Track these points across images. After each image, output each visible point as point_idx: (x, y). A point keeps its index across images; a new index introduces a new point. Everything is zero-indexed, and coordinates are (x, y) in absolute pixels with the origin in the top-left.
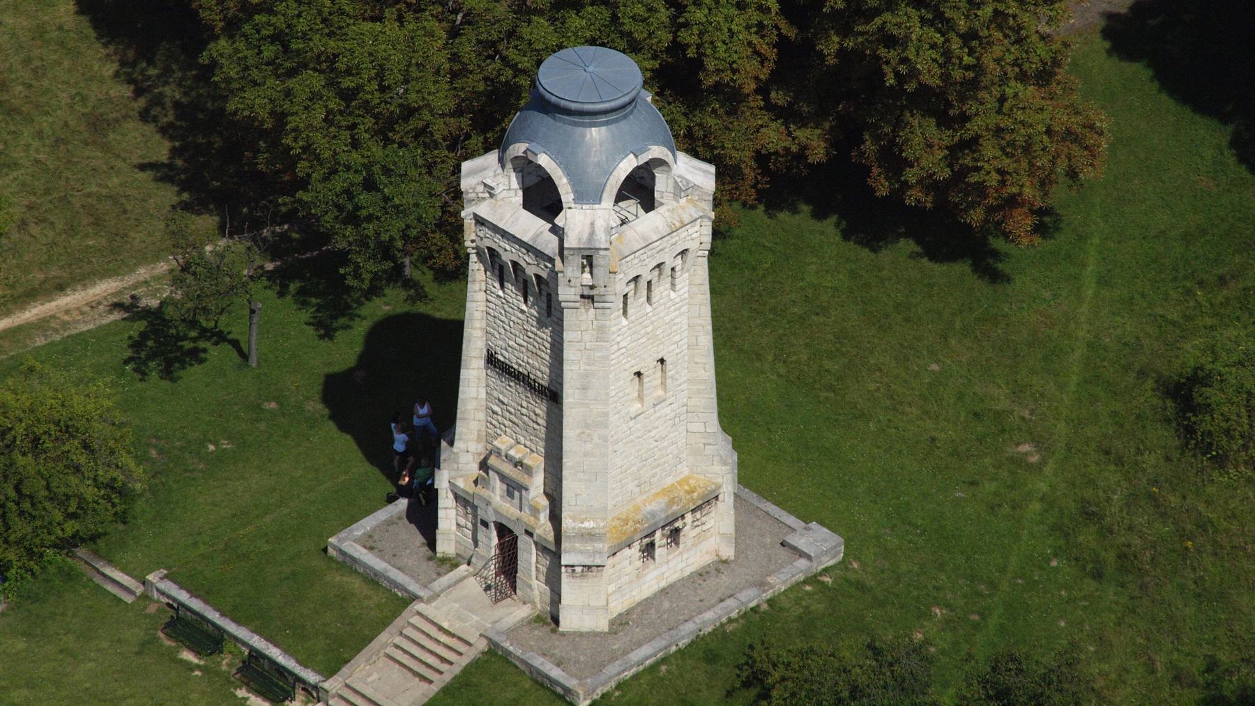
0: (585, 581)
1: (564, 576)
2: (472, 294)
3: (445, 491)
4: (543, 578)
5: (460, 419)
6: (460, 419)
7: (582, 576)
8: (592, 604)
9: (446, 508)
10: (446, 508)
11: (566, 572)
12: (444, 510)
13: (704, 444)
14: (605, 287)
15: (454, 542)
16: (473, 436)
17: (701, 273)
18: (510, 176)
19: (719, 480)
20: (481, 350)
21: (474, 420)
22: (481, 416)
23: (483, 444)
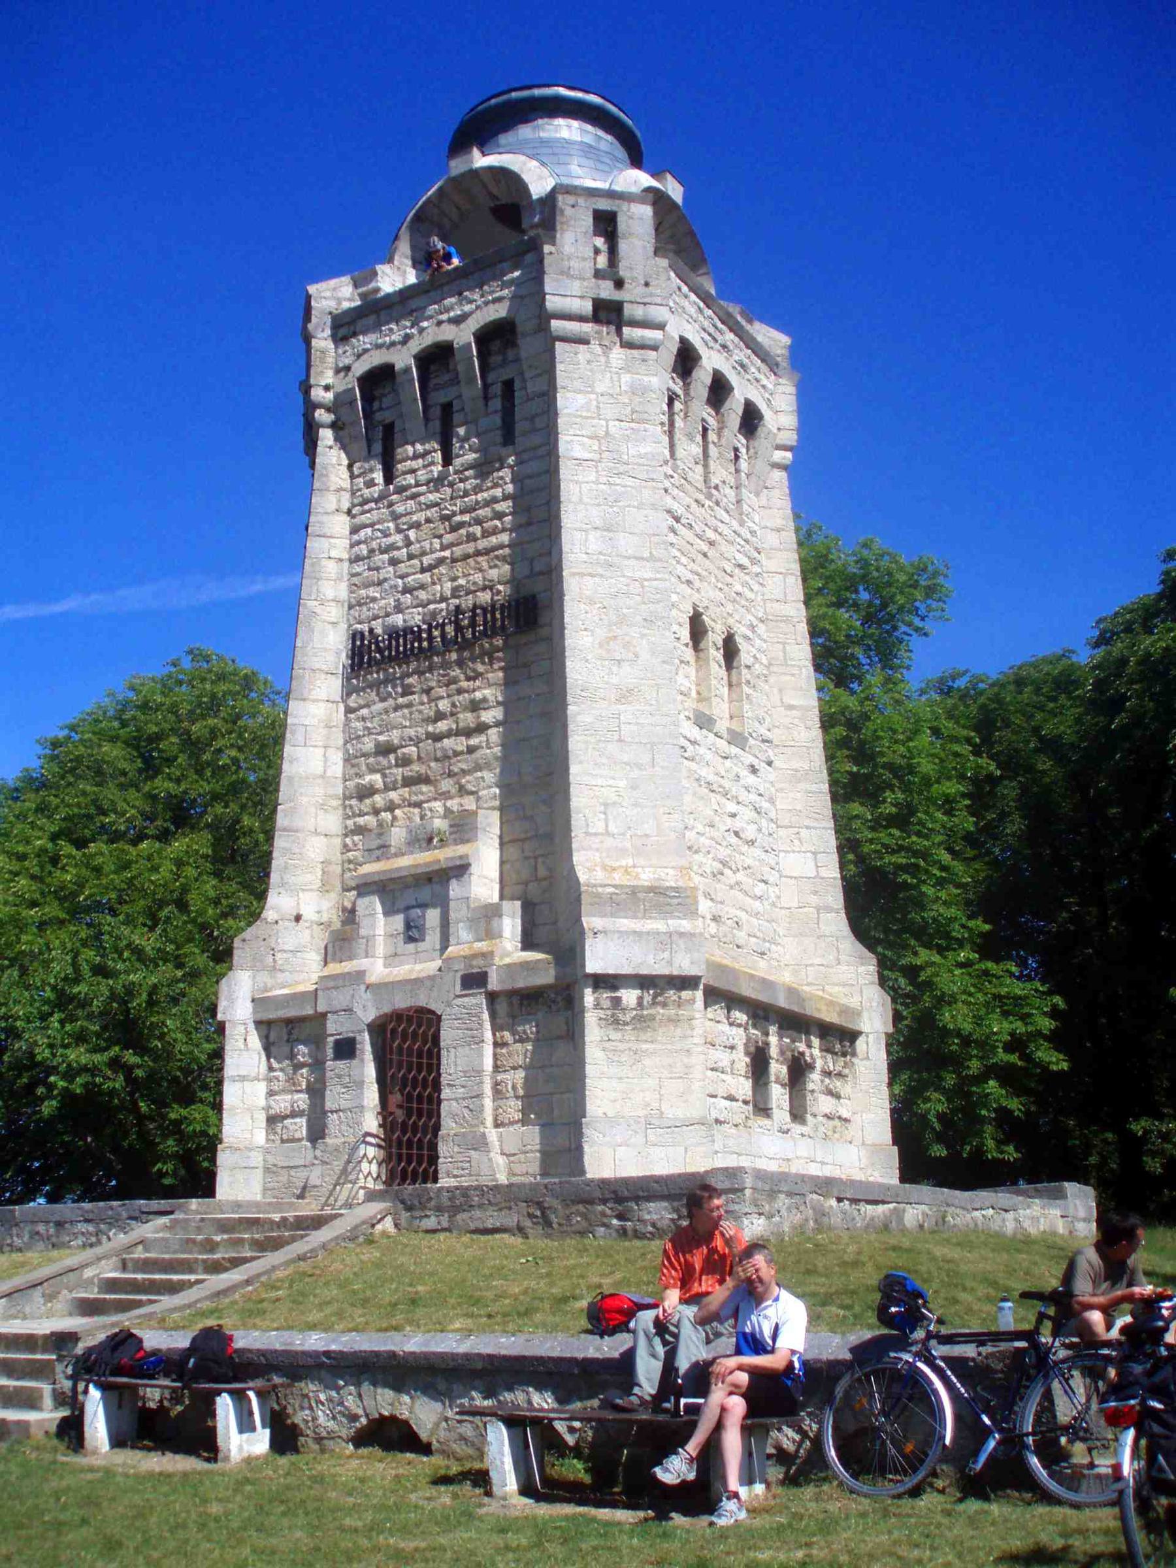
0: (648, 1035)
1: (591, 1019)
2: (320, 518)
3: (241, 1029)
4: (513, 1109)
5: (285, 830)
6: (285, 830)
7: (639, 1019)
8: (669, 1113)
9: (243, 1079)
10: (243, 1079)
11: (597, 1006)
12: (238, 1085)
13: (818, 909)
14: (647, 284)
15: (259, 1173)
16: (309, 877)
17: (779, 503)
18: (405, 272)
19: (854, 1002)
20: (338, 653)
21: (316, 833)
22: (332, 822)
23: (333, 896)
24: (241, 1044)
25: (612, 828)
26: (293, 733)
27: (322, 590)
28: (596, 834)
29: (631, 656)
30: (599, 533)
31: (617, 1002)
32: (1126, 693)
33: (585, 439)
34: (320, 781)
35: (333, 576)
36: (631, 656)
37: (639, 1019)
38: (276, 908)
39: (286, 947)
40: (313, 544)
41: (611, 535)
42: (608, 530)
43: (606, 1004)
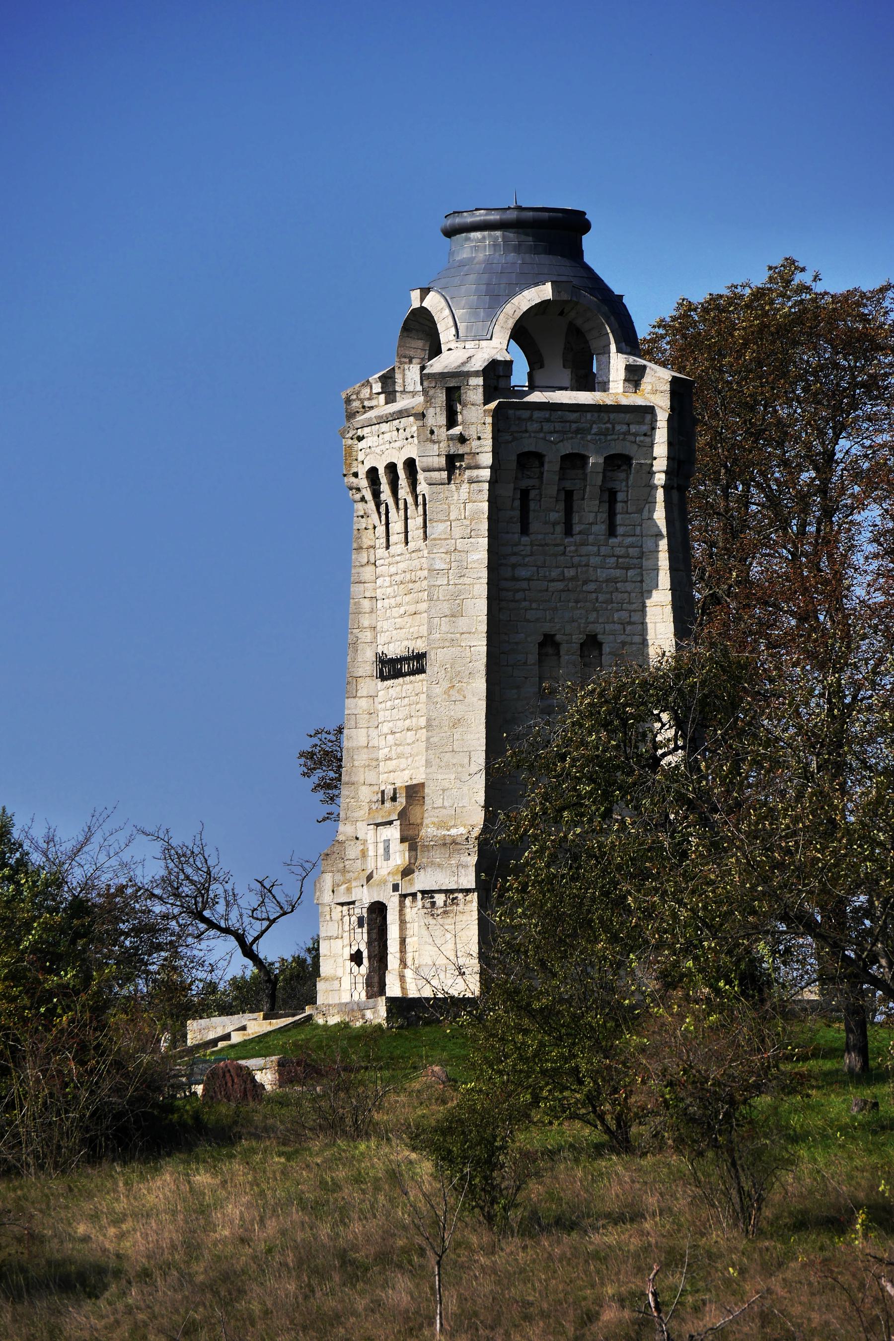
5: (347, 784)
6: (347, 784)
7: (445, 912)
9: (330, 938)
10: (330, 938)
24: (328, 917)
25: (446, 804)
26: (349, 720)
27: (362, 621)
28: (437, 808)
29: (461, 698)
30: (448, 619)
31: (433, 904)
32: (31, 934)
33: (443, 555)
34: (365, 750)
35: (368, 610)
36: (461, 698)
37: (445, 912)
38: (344, 833)
39: (351, 857)
40: (355, 589)
41: (454, 619)
42: (452, 616)
43: (429, 905)
